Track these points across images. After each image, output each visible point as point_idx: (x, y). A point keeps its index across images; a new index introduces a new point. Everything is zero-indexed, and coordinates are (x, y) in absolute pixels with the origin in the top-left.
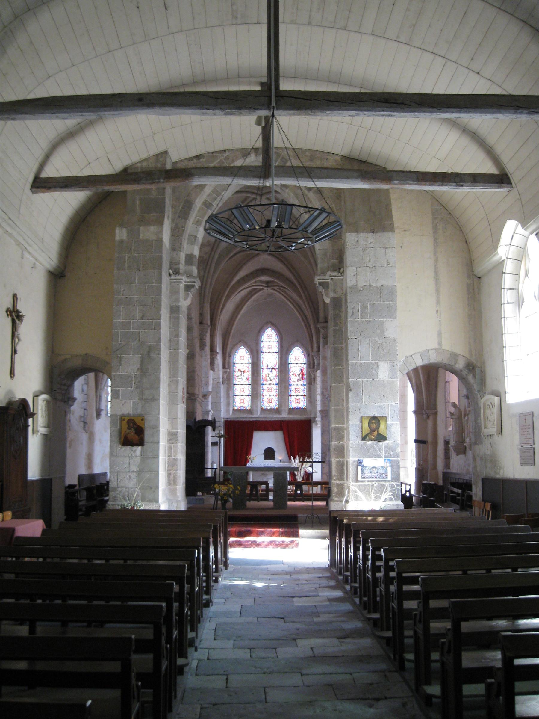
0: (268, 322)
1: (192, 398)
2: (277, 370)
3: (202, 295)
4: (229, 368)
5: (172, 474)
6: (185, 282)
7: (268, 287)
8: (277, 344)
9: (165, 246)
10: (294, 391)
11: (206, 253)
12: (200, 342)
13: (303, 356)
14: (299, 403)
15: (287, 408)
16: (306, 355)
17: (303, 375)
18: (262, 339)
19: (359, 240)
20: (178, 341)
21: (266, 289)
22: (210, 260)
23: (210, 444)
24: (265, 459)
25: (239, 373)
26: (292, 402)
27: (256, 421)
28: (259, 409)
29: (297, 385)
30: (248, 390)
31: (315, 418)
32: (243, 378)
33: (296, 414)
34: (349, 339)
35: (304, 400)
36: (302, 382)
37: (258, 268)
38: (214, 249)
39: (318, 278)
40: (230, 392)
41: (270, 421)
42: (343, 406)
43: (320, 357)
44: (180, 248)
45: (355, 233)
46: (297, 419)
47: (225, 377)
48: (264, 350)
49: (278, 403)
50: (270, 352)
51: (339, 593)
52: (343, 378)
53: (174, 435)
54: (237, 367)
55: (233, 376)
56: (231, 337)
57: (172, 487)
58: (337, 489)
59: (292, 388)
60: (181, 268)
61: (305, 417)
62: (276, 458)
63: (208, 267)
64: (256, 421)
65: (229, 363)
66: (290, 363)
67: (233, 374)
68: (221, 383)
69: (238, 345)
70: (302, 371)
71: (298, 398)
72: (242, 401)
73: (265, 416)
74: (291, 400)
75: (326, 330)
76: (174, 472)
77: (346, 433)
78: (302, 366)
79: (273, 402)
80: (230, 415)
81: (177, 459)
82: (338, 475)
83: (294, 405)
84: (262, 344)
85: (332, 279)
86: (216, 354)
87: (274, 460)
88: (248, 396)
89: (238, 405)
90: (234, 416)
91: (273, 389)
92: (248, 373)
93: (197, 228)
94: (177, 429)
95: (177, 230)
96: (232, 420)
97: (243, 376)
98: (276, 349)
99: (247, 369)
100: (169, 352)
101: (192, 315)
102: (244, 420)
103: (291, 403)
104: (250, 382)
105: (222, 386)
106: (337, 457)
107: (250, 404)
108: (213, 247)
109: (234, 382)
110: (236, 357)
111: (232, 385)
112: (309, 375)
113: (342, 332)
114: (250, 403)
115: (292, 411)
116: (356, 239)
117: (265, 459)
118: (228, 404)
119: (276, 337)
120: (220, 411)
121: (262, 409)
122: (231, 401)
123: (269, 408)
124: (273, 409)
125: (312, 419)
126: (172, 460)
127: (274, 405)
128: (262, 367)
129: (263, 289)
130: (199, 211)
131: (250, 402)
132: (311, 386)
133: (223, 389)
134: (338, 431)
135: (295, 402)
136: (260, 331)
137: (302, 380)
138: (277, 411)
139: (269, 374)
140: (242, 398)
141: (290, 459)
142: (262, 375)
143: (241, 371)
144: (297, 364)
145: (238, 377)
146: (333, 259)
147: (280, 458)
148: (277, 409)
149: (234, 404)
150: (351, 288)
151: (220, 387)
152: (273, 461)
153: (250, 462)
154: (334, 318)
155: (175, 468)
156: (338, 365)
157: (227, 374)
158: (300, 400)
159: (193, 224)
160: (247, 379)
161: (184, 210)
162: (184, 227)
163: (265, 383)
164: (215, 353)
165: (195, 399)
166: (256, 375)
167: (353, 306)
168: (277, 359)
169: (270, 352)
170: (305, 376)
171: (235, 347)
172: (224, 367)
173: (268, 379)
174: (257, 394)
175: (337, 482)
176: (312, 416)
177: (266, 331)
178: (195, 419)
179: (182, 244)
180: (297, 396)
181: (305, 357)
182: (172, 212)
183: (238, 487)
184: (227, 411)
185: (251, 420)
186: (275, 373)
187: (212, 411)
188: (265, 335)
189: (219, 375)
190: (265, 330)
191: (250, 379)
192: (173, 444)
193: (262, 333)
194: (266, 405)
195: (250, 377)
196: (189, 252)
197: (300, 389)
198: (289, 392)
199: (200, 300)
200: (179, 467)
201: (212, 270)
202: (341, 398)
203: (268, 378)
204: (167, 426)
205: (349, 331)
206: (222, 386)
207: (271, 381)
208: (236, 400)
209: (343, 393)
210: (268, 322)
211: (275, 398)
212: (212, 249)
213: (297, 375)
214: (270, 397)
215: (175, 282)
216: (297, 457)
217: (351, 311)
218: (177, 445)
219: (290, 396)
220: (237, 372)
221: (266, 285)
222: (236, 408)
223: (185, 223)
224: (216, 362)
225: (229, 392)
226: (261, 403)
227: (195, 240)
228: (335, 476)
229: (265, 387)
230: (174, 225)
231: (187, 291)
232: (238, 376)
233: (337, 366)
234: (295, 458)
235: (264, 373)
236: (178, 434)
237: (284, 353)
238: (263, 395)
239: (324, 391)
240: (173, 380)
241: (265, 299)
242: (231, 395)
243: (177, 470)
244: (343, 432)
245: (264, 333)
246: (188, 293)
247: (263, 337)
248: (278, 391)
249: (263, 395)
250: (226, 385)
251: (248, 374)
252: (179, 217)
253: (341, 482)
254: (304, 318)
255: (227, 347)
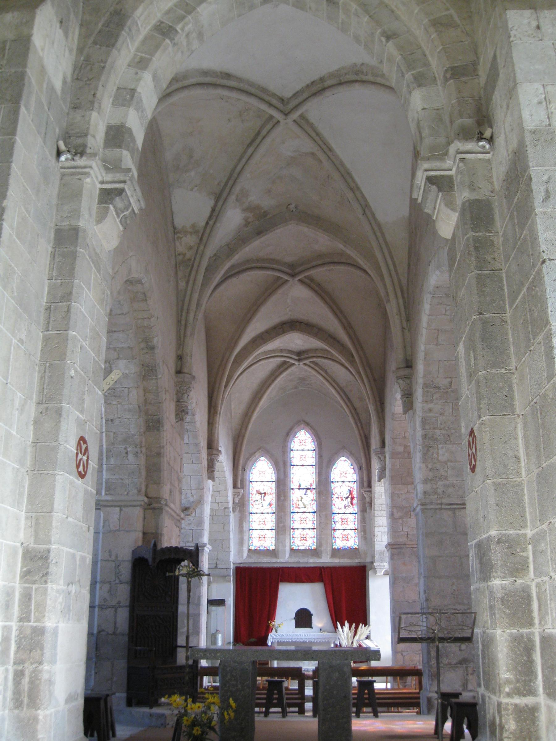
0: (300, 421)
1: (155, 505)
2: (314, 491)
3: (183, 322)
4: (243, 487)
5: (27, 673)
6: (102, 183)
7: (299, 360)
8: (313, 454)
9: (43, 70)
10: (340, 522)
11: (191, 248)
12: (177, 406)
13: (353, 471)
14: (348, 540)
15: (329, 549)
16: (356, 469)
17: (352, 498)
18: (292, 446)
19: (542, 25)
20: (68, 311)
21: (296, 363)
22: (197, 260)
23: (204, 602)
24: (296, 627)
25: (258, 497)
26: (337, 539)
27: (283, 568)
28: (288, 549)
29: (344, 513)
30: (270, 521)
31: (372, 563)
32: (263, 503)
33: (343, 556)
34: (544, 262)
35: (354, 536)
36: (351, 510)
37: (284, 318)
38: (205, 238)
39: (426, 165)
40: (244, 524)
41: (304, 568)
42: (519, 474)
43: (385, 457)
44: (92, 103)
45: (530, 11)
46: (345, 565)
47: (237, 501)
48: (294, 462)
49: (315, 541)
50: (303, 465)
51: (111, 274)
52: (512, 399)
53: (41, 558)
54: (254, 488)
55: (249, 500)
56: (245, 442)
57: (25, 713)
58: (517, 722)
59: (337, 518)
60: (89, 145)
61: (357, 561)
62: (313, 625)
63: (193, 273)
64: (283, 567)
65: (242, 481)
66: (334, 480)
67: (249, 497)
68: (231, 509)
69: (257, 455)
70: (351, 493)
71: (346, 532)
72: (262, 538)
73: (296, 560)
74: (336, 536)
75: (408, 381)
76: (31, 668)
77: (534, 554)
78: (351, 484)
79: (308, 539)
80: (245, 559)
81: (44, 627)
82: (518, 681)
83: (339, 544)
84: (292, 454)
85: (462, 160)
86: (217, 453)
87: (311, 627)
88: (272, 530)
89: (256, 543)
90: (250, 561)
91: (308, 520)
92: (271, 496)
93: (137, 73)
94: (50, 543)
95: (89, 67)
96: (247, 566)
97: (264, 500)
98: (313, 461)
99: (270, 491)
100: (44, 337)
101: (155, 340)
102: (264, 566)
103: (335, 540)
104: (274, 509)
105: (232, 515)
106: (511, 625)
107: (274, 542)
108: (203, 235)
109: (251, 509)
110: (253, 472)
111: (247, 514)
112: (362, 499)
113: (501, 280)
114: (273, 540)
115: (336, 552)
116: (534, 24)
117: (296, 627)
118: (241, 542)
119: (313, 443)
120: (229, 552)
121: (292, 550)
122: (246, 538)
123: (302, 548)
124: (309, 549)
125: (367, 565)
126: (28, 631)
127: (310, 543)
128: (292, 487)
129: (293, 364)
130: (144, 42)
131: (274, 539)
132: (365, 514)
133: (232, 518)
134: (509, 547)
135: (341, 538)
136: (289, 434)
137: (351, 506)
138: (315, 552)
139: (302, 498)
140: (262, 533)
141: (336, 627)
142: (291, 498)
143: (261, 494)
144: (343, 482)
145: (257, 502)
146: (461, 116)
147: (320, 625)
148: (315, 549)
149: (250, 541)
150: (534, 132)
151: (229, 516)
152: (309, 629)
153: (274, 630)
154: (476, 249)
155: (35, 655)
156: (495, 365)
157: (240, 496)
158: (349, 536)
159: (129, 66)
160: (270, 505)
161: (108, 29)
162: (105, 62)
163: (296, 510)
164: (214, 452)
165: (161, 509)
166: (282, 498)
167: (545, 178)
168: (314, 476)
169: (303, 465)
170: (355, 501)
171: (252, 457)
172: (235, 486)
173: (301, 505)
174: (284, 526)
175: (517, 700)
176: (368, 560)
177: (298, 434)
178: (155, 545)
179: (98, 95)
180: (344, 530)
181: (355, 472)
182: (80, 35)
183: (231, 701)
184: (240, 552)
185: (276, 566)
186: (312, 495)
187: (208, 546)
188: (296, 440)
189: (227, 497)
190: (296, 433)
191: (274, 506)
192: (34, 587)
193: (291, 436)
194: (299, 544)
195: (274, 501)
196: (115, 121)
197: (349, 520)
198: (332, 525)
199: (178, 332)
200: (47, 654)
201: (200, 278)
202: (511, 453)
203: (300, 503)
204: (22, 536)
205: (541, 239)
206: (232, 515)
207: (305, 507)
208: (253, 536)
209: (516, 439)
210: (300, 421)
211: (312, 533)
212: (201, 239)
213: (344, 499)
214: (305, 532)
215: (72, 174)
216: (347, 624)
217: (542, 189)
218: (46, 589)
219: (335, 530)
220: (254, 495)
221: (297, 358)
222: (253, 548)
223: (108, 54)
224: (217, 466)
225: (242, 523)
226: (290, 540)
227: (132, 96)
228: (508, 681)
229: (296, 517)
230: (82, 58)
231: (106, 202)
232: (257, 500)
233: (492, 368)
234: (342, 625)
235: (295, 496)
236: (52, 555)
237: (324, 465)
238: (293, 529)
239: (395, 511)
240: (47, 409)
241: (296, 387)
242: (245, 529)
243: (41, 663)
244: (525, 550)
245: (294, 436)
246: (108, 207)
247: (292, 443)
248: (315, 522)
249: (293, 529)
250: (237, 512)
251: (271, 498)
252: (95, 43)
253: (528, 701)
254: (353, 411)
255: (239, 457)
